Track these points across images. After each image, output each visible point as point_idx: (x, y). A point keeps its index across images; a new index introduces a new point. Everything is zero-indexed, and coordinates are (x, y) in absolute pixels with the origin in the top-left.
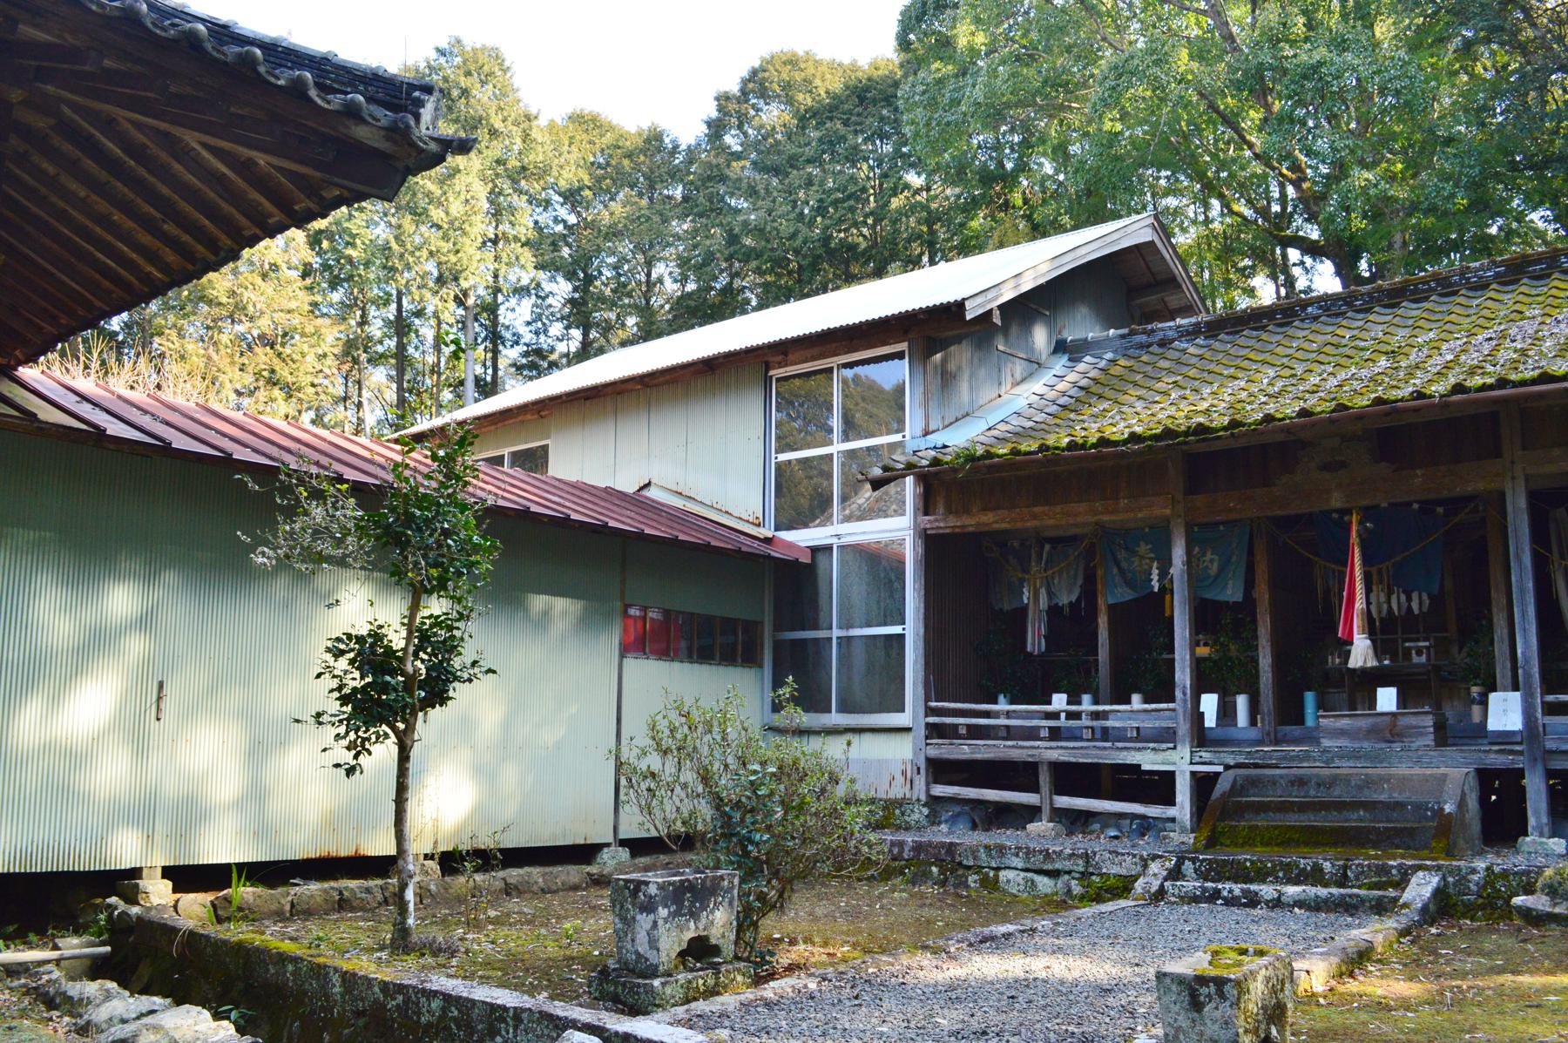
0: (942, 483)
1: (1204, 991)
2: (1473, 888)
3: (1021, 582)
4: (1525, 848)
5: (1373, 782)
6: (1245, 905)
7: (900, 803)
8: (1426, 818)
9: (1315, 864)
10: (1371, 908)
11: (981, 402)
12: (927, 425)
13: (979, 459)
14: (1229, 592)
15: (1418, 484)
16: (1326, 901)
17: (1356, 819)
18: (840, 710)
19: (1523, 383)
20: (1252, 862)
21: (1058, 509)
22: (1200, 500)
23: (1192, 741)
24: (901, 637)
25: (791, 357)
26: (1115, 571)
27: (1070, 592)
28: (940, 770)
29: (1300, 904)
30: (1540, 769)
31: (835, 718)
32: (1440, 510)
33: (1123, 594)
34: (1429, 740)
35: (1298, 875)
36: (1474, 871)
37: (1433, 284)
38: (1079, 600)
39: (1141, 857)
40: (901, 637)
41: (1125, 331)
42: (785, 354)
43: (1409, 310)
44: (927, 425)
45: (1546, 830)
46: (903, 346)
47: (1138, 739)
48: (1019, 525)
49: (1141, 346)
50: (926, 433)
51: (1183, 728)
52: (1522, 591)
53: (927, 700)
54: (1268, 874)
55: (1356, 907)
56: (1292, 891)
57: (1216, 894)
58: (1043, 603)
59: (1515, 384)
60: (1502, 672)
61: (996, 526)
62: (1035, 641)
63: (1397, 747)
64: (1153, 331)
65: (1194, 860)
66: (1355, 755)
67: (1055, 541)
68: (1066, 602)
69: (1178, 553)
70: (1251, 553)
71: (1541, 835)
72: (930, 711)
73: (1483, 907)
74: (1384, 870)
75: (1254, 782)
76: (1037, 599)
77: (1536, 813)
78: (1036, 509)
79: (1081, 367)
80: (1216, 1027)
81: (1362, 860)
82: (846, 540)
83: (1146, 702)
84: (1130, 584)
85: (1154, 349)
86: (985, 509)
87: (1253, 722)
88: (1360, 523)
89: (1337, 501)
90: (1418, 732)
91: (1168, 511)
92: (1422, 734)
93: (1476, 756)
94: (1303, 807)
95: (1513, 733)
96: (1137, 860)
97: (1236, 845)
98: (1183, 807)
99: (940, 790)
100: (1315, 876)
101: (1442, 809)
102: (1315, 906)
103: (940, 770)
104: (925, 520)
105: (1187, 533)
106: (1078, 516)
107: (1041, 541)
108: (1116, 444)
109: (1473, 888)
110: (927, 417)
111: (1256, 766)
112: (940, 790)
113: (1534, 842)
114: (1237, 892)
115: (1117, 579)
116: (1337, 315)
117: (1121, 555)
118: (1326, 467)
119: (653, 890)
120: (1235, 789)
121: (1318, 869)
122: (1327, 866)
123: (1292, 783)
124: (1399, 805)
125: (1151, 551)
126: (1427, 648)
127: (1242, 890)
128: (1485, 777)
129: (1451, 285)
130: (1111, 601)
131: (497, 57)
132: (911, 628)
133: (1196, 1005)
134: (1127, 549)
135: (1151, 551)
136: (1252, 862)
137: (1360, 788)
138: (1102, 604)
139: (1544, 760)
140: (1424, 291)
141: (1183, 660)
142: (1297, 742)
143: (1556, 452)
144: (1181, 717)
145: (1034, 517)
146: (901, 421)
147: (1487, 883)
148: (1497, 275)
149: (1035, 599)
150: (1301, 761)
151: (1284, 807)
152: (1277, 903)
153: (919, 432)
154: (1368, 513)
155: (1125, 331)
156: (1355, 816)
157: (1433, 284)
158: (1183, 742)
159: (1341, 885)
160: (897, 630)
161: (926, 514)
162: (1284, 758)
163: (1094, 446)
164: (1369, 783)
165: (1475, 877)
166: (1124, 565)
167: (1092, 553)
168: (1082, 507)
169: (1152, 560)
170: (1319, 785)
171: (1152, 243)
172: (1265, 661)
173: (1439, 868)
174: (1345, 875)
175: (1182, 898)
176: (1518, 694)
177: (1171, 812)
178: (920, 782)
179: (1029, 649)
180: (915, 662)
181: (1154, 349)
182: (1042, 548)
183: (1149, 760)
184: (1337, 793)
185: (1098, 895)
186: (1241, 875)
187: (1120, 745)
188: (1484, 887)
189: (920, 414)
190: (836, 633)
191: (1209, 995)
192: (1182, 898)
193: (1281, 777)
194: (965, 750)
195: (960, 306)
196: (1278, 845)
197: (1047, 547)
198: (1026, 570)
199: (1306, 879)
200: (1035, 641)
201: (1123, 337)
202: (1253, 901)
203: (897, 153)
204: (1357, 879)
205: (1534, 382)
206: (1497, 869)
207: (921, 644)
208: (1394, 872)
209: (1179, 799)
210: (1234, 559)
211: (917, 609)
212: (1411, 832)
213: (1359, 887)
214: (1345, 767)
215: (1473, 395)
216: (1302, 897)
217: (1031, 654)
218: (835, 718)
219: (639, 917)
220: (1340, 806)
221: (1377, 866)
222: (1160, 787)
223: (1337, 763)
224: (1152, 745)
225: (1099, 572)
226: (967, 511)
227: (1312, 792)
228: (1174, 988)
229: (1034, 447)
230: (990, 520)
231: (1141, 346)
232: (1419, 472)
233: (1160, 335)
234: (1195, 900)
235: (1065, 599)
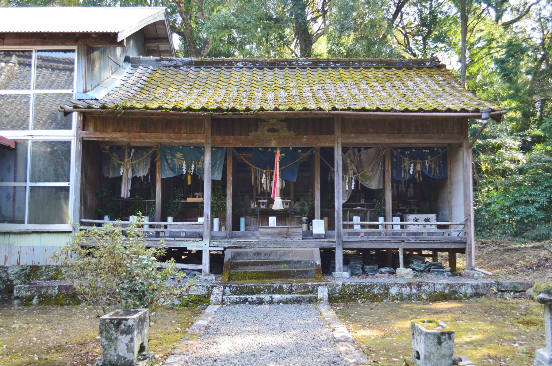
0: (91, 116)
1: (443, 337)
2: (338, 291)
3: (120, 165)
4: (336, 276)
5: (286, 254)
6: (258, 304)
8: (308, 266)
9: (280, 286)
10: (307, 301)
12: (86, 87)
13: (128, 108)
14: (216, 176)
15: (304, 141)
16: (290, 300)
17: (283, 268)
18: (30, 222)
19: (356, 110)
20: (255, 287)
21: (153, 135)
22: (218, 138)
24: (67, 189)
25: (6, 41)
26: (166, 164)
27: (143, 171)
29: (279, 302)
30: (341, 248)
31: (27, 226)
32: (300, 151)
33: (169, 174)
34: (300, 237)
35: (273, 291)
36: (338, 285)
37: (286, 63)
38: (148, 175)
39: (207, 287)
40: (67, 189)
41: (158, 58)
42: (3, 39)
44: (86, 87)
45: (342, 269)
46: (75, 47)
47: (185, 237)
48: (133, 140)
49: (166, 66)
50: (85, 92)
51: (206, 232)
52: (338, 184)
53: (80, 219)
54: (261, 291)
55: (301, 301)
56: (277, 297)
57: (246, 300)
58: (130, 176)
59: (354, 110)
61: (120, 139)
62: (125, 192)
63: (288, 240)
64: (171, 60)
65: (230, 287)
66: (276, 243)
67: (136, 148)
68: (142, 176)
69: (207, 159)
70: (226, 160)
71: (340, 271)
72: (82, 224)
73: (341, 298)
74: (306, 287)
75: (239, 254)
76: (127, 173)
77: (339, 263)
78: (142, 134)
79: (139, 70)
80: (446, 350)
81: (296, 283)
82: (36, 139)
83: (174, 221)
84: (172, 170)
85: (172, 68)
86: (114, 131)
87: (220, 230)
88: (281, 153)
89: (273, 144)
90: (296, 234)
91: (203, 141)
92: (298, 235)
93: (319, 243)
94: (262, 264)
95: (321, 235)
96: (205, 288)
97: (238, 280)
98: (206, 264)
100: (280, 291)
101: (316, 263)
102: (287, 302)
104: (84, 134)
105: (212, 150)
106: (148, 139)
107: (130, 148)
108: (195, 110)
109: (338, 291)
110: (86, 84)
111: (237, 247)
113: (339, 274)
114: (255, 299)
115: (167, 167)
116: (250, 68)
117: (169, 157)
118: (269, 130)
119: (130, 323)
120: (234, 257)
121: (281, 288)
122: (285, 286)
123: (255, 254)
124: (299, 262)
125: (183, 156)
126: (290, 202)
127: (257, 298)
129: (292, 65)
130: (163, 177)
132: (74, 183)
133: (440, 343)
134: (171, 154)
135: (183, 156)
136: (255, 287)
137: (281, 256)
138: (159, 177)
139: (343, 245)
140: (282, 65)
141: (207, 203)
142: (240, 237)
143: (353, 135)
144: (206, 227)
145: (141, 137)
146: (71, 83)
147: (342, 289)
148: (309, 65)
149: (126, 173)
150: (255, 245)
151: (255, 264)
152: (271, 302)
153: (81, 90)
154: (283, 150)
155: (158, 58)
156: (282, 266)
157: (286, 63)
158: (207, 238)
159: (290, 293)
160: (65, 184)
161: (83, 130)
162: (248, 244)
163: (185, 110)
164: (284, 254)
165: (338, 288)
166: (169, 161)
167: (154, 155)
168: (164, 135)
169: (183, 160)
170: (265, 255)
171: (164, 20)
173: (326, 285)
174: (292, 290)
175: (231, 303)
176: (323, 221)
177: (199, 267)
179: (122, 196)
180: (75, 200)
181: (172, 68)
182: (131, 151)
183: (192, 246)
184: (272, 258)
185: (187, 304)
186: (251, 292)
187: (178, 239)
188: (341, 291)
189: (82, 82)
190: (29, 184)
191: (445, 339)
192: (231, 303)
193: (250, 252)
195: (115, 35)
196: (255, 279)
197: (133, 150)
198: (123, 160)
199: (276, 292)
200: (125, 192)
201: (157, 60)
202: (261, 302)
204: (296, 291)
205: (360, 110)
206: (346, 284)
207: (78, 192)
208: (310, 287)
209: (204, 261)
210: (218, 163)
211: (76, 175)
212: (306, 272)
213: (297, 294)
214: (272, 248)
215: (339, 112)
216: (281, 299)
217: (123, 198)
218: (27, 226)
219: (120, 337)
220: (277, 263)
221: (304, 285)
222: (197, 257)
223: (269, 246)
224: (192, 239)
225: (158, 164)
226: (104, 131)
227: (262, 258)
228: (432, 338)
229: (142, 106)
230: (107, 136)
231: (166, 66)
232: (305, 137)
233: (174, 63)
234: (237, 303)
235: (142, 173)
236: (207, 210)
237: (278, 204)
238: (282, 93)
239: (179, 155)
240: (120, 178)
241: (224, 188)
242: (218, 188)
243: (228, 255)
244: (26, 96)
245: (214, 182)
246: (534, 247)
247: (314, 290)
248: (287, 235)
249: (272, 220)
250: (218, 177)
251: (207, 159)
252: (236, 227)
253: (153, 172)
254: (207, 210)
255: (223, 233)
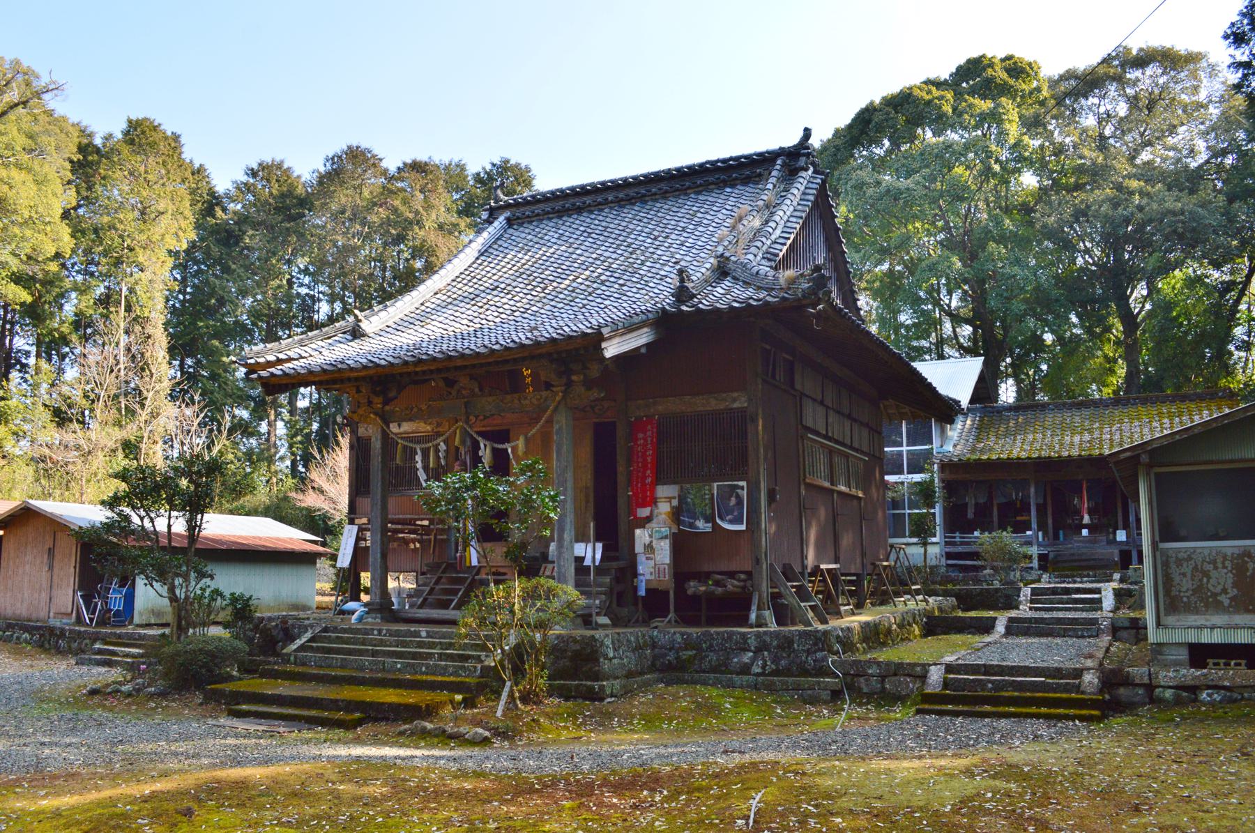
7: (936, 566)
11: (154, 583)
17: (1092, 563)
23: (654, 585)
28: (949, 556)
33: (1003, 500)
43: (1086, 412)
60: (1120, 523)
62: (970, 515)
69: (1032, 490)
89: (1080, 477)
98: (1035, 564)
99: (950, 562)
100: (1088, 576)
103: (949, 556)
112: (950, 562)
120: (1056, 557)
128: (1122, 552)
131: (528, 170)
149: (971, 501)
172: (1050, 521)
178: (943, 560)
194: (960, 549)
200: (970, 515)
203: (1091, 234)
214: (1084, 550)
235: (982, 501)
236: (1034, 526)
237: (1086, 519)
238: (1087, 437)
239: (1009, 486)
240: (966, 505)
241: (1046, 508)
242: (1041, 510)
243: (1051, 555)
244: (900, 454)
245: (1038, 506)
246: (558, 460)
247: (1111, 575)
248: (1095, 542)
249: (1085, 532)
250: (1041, 501)
251: (1032, 490)
252: (1056, 537)
253: (991, 498)
254: (1034, 526)
255: (1047, 542)
